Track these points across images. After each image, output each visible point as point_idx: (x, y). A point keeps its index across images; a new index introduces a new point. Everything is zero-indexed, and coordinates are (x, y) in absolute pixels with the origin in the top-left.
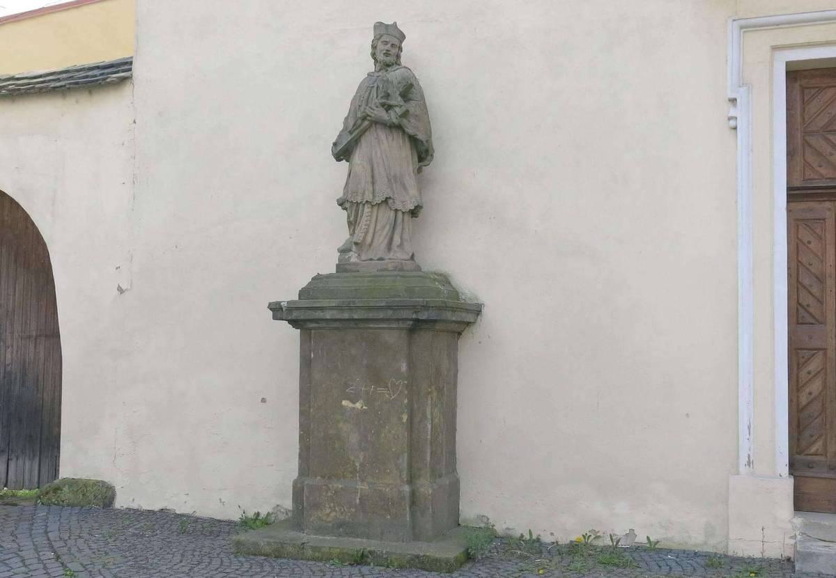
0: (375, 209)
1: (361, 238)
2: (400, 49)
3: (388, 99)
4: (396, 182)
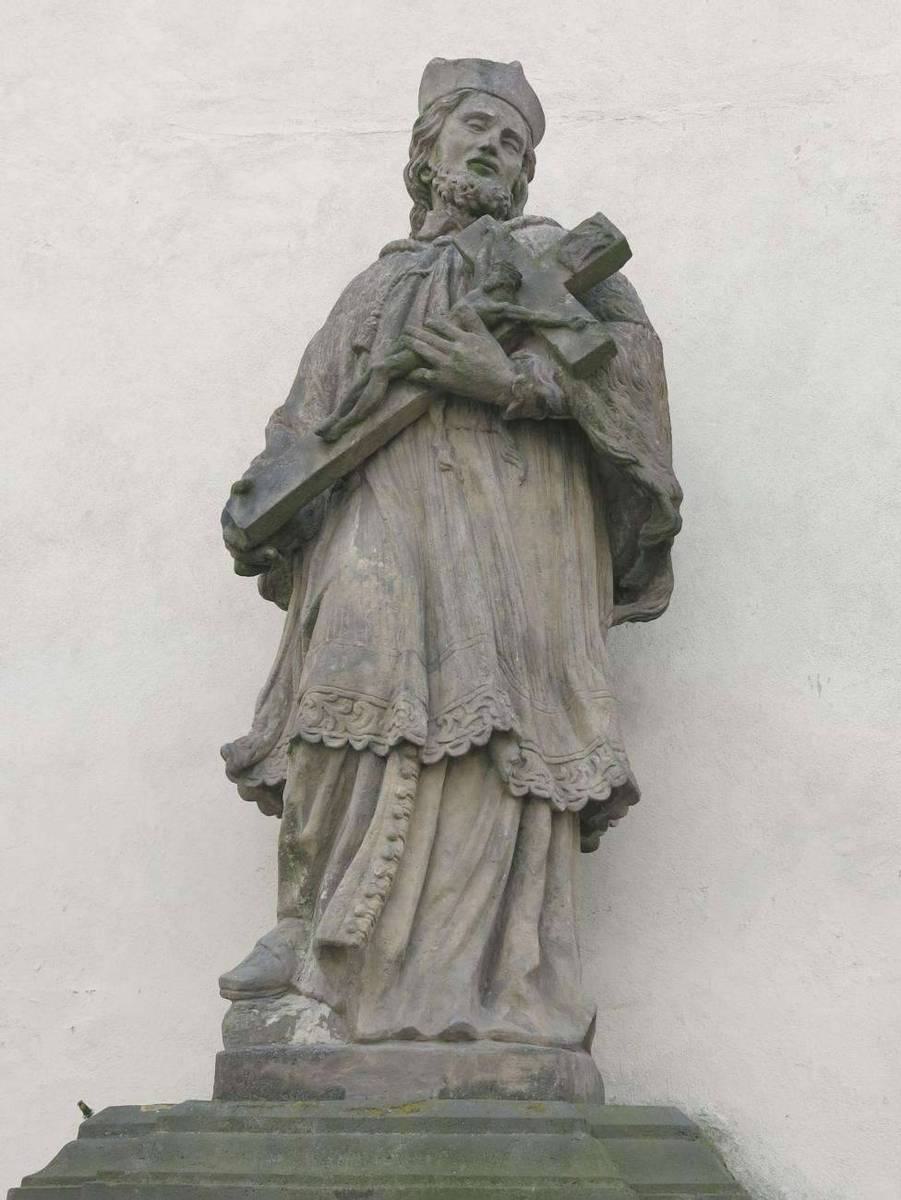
0: (434, 784)
1: (364, 924)
2: (529, 162)
3: (515, 302)
4: (532, 671)
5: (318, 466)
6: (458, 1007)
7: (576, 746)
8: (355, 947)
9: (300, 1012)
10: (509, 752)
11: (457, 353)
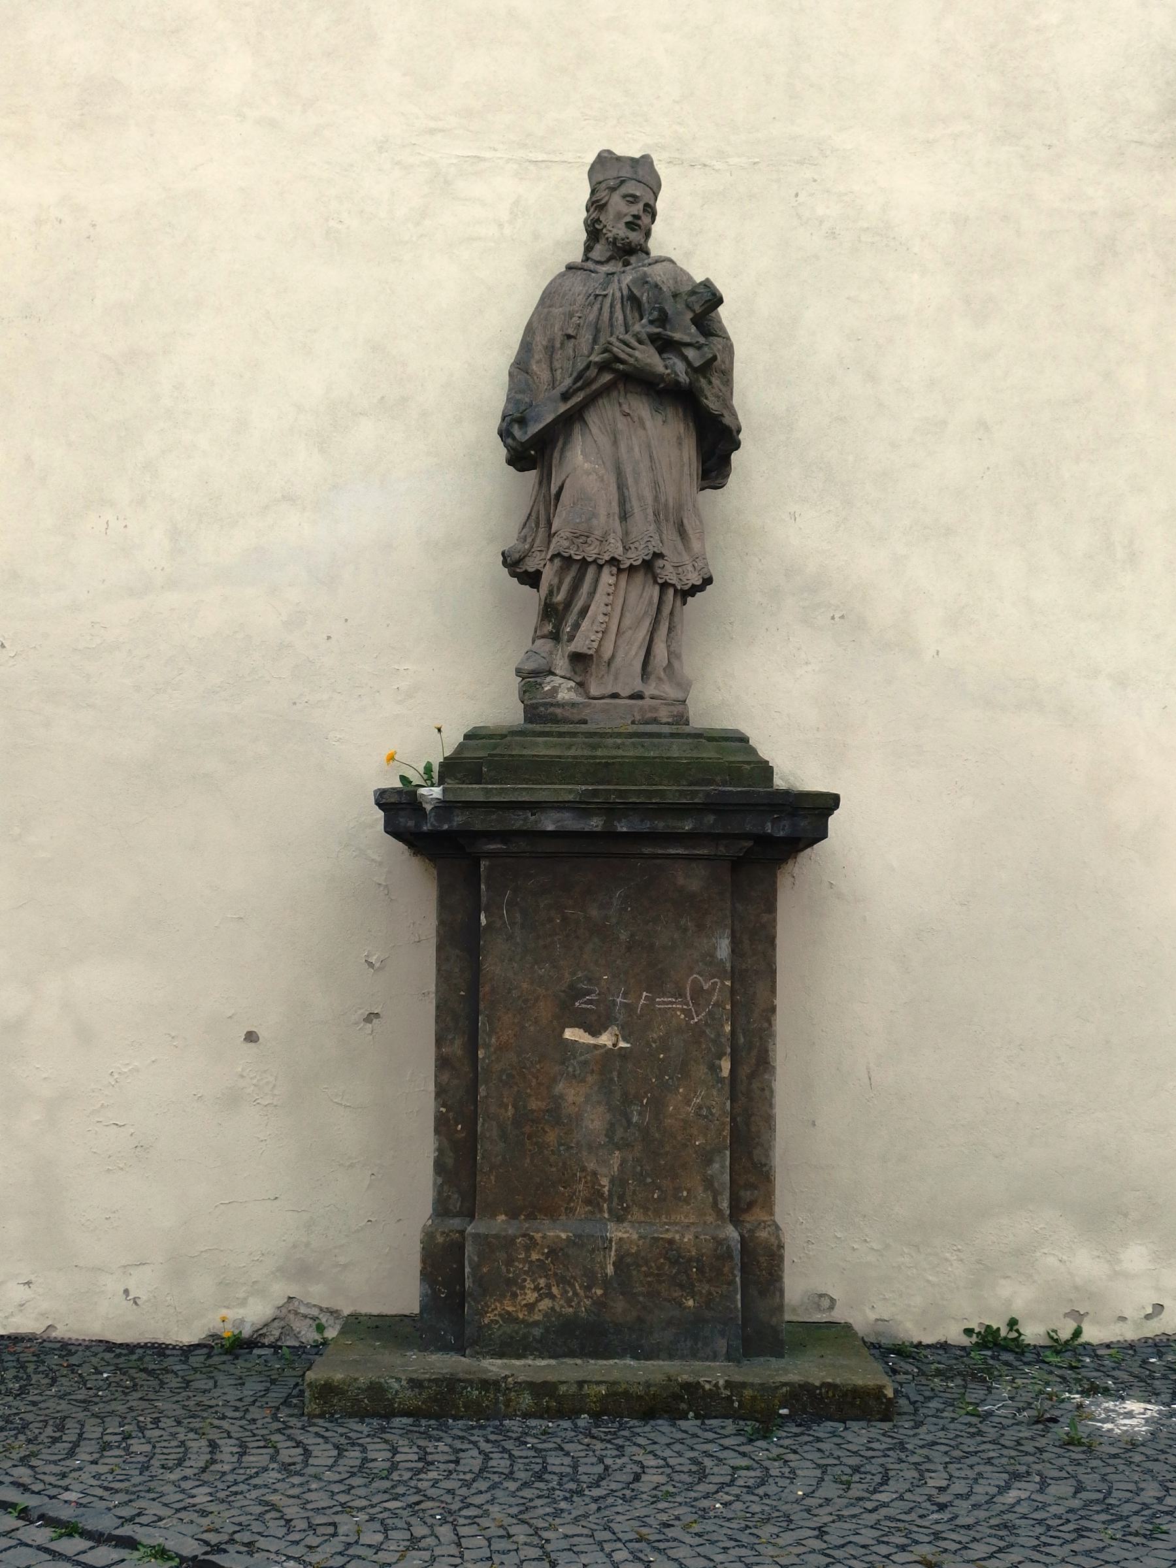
0: (624, 577)
1: (595, 645)
3: (664, 328)
5: (561, 410)
6: (631, 682)
7: (686, 558)
8: (592, 655)
9: (560, 684)
10: (660, 563)
11: (636, 358)
